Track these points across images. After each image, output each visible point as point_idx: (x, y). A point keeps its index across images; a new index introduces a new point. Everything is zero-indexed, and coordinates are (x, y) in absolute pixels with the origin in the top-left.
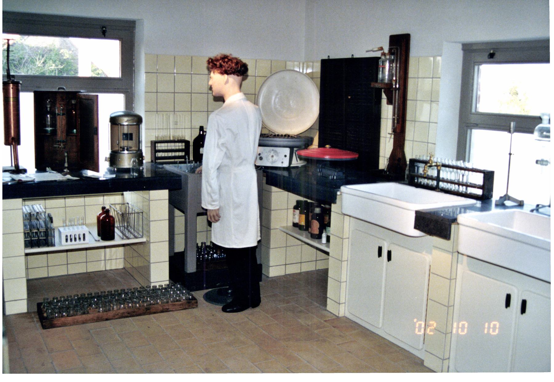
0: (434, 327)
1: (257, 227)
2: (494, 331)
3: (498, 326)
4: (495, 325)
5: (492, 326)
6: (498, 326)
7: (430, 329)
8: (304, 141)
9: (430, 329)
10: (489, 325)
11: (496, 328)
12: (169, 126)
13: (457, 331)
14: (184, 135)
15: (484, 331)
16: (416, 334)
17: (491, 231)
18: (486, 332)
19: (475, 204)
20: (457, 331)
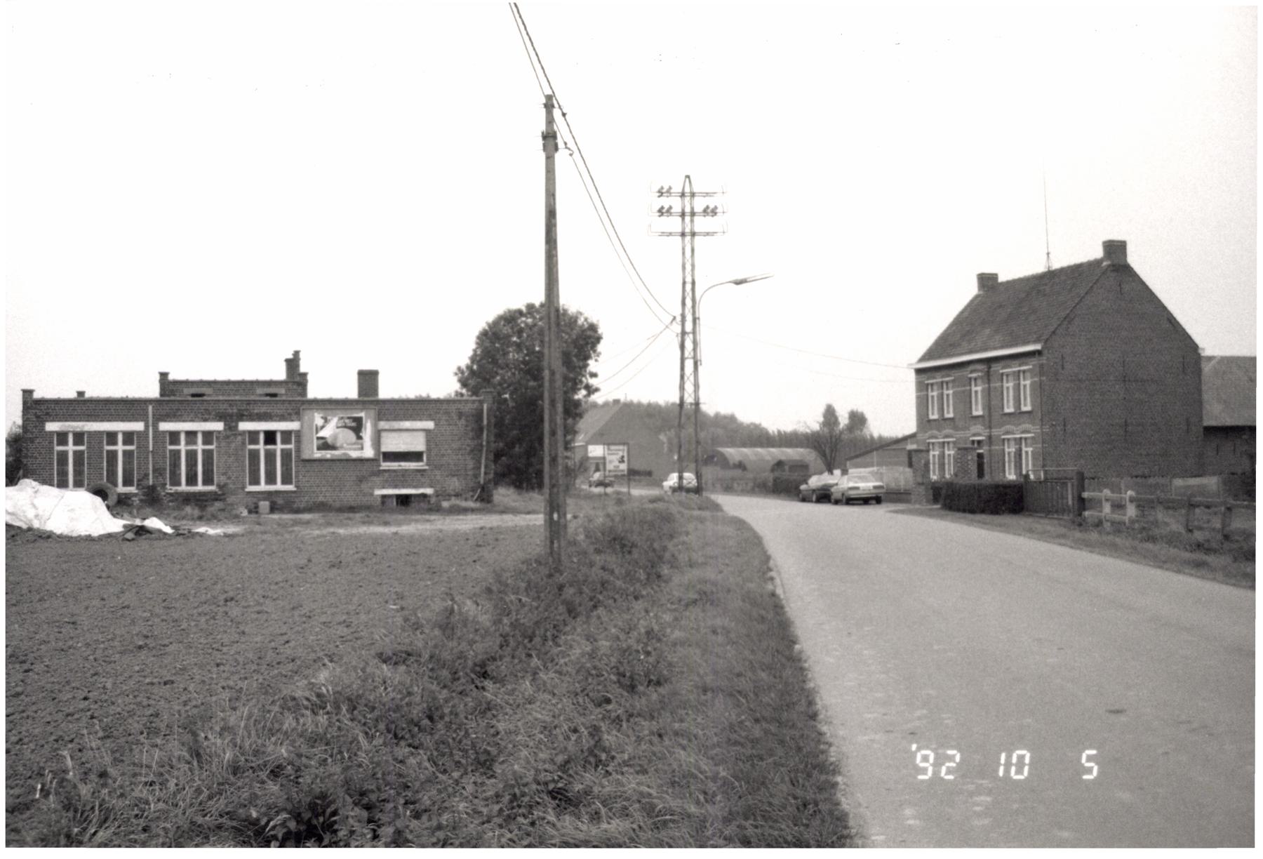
0: (954, 761)
1: (979, 522)
2: (1019, 771)
3: (1027, 760)
4: (1021, 758)
5: (1014, 760)
6: (1027, 760)
10: (1009, 757)
11: (1024, 765)
12: (689, 387)
13: (1007, 771)
14: (689, 399)
15: (997, 771)
16: (942, 779)
18: (1001, 773)
20: (1007, 771)
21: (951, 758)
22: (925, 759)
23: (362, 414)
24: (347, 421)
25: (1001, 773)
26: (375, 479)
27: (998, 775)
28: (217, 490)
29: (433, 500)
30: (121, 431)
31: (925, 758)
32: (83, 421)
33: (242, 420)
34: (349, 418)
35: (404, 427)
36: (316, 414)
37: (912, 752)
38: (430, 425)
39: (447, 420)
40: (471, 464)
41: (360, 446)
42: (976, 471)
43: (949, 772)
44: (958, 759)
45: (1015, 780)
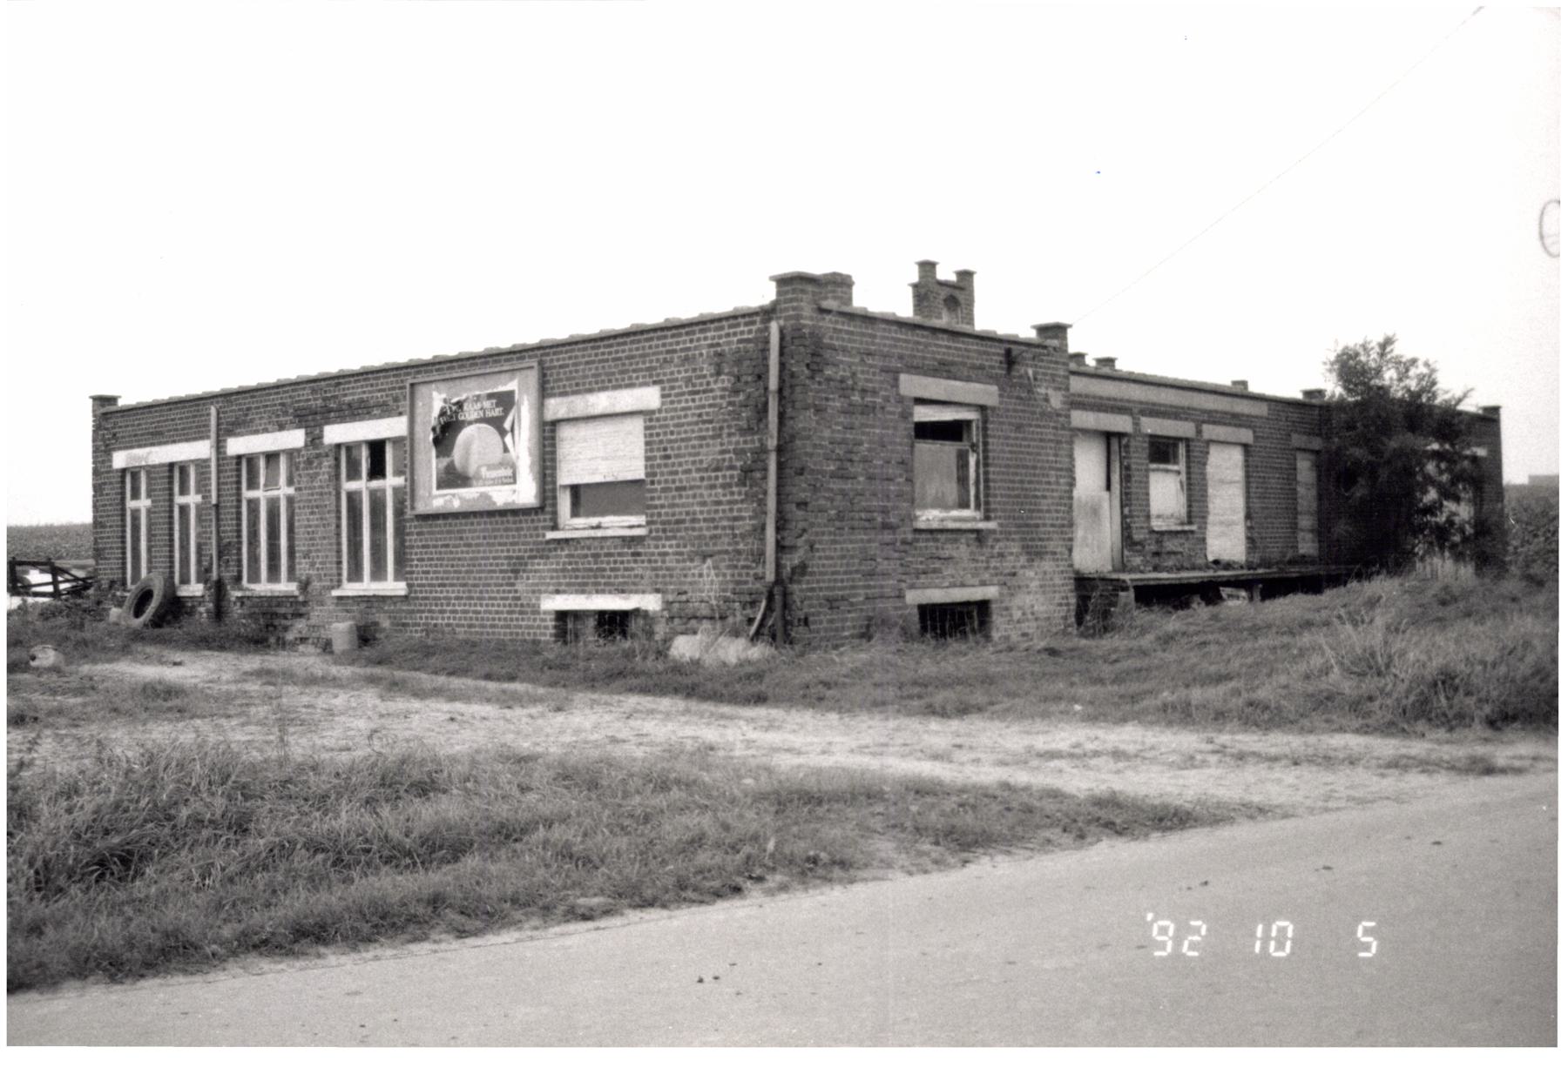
2: (1281, 946)
3: (1290, 934)
4: (1282, 930)
5: (1274, 934)
6: (1290, 934)
7: (1164, 949)
8: (819, 791)
9: (1164, 949)
10: (1267, 931)
13: (1265, 947)
16: (1184, 955)
17: (1104, 465)
18: (1257, 949)
19: (772, 437)
20: (1265, 947)
21: (1197, 931)
22: (1163, 930)
23: (512, 385)
24: (487, 404)
25: (1257, 949)
26: (540, 565)
27: (1253, 952)
28: (297, 593)
29: (661, 630)
30: (263, 453)
31: (1162, 930)
32: (145, 446)
33: (328, 422)
34: (490, 396)
35: (598, 410)
36: (435, 394)
37: (1146, 923)
38: (649, 397)
39: (688, 380)
40: (747, 510)
41: (509, 472)
42: (1159, 421)
43: (1192, 946)
44: (1203, 931)
45: (1275, 958)
